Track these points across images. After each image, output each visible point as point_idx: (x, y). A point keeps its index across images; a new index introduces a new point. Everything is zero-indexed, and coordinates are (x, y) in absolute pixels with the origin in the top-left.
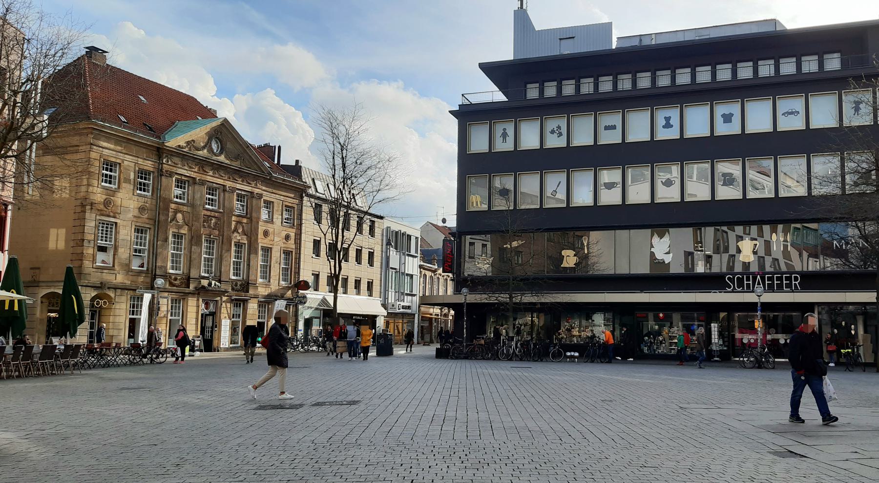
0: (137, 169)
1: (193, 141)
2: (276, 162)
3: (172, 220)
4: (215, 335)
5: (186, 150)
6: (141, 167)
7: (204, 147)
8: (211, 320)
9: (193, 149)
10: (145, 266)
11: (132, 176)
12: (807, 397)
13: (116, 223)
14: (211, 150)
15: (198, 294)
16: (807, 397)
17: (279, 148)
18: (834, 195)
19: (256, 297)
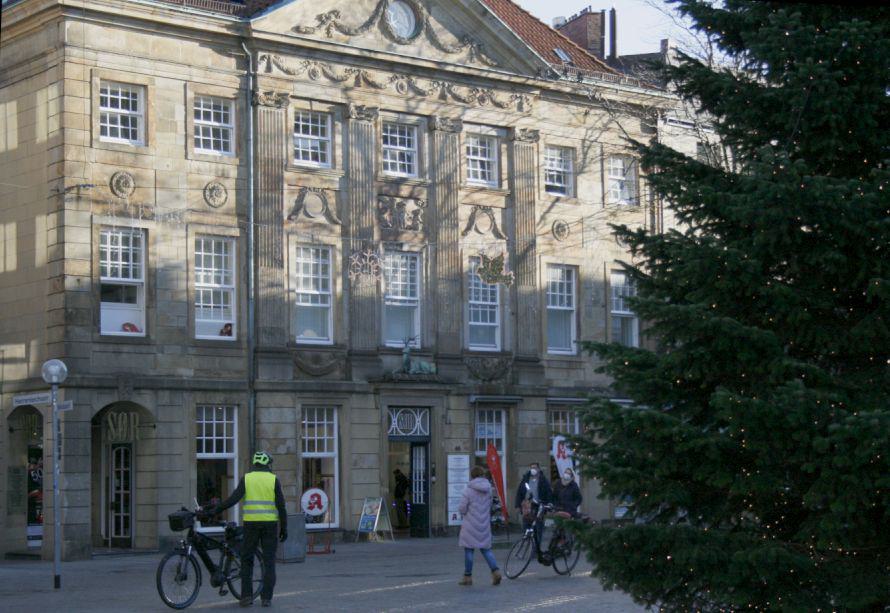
0: (191, 95)
1: (335, 13)
2: (607, 52)
3: (295, 211)
4: (436, 495)
5: (320, 35)
6: (204, 90)
7: (367, 25)
8: (422, 456)
9: (334, 32)
10: (234, 331)
11: (179, 117)
12: (621, 268)
13: (146, 231)
14: (386, 30)
15: (376, 392)
16: (621, 268)
17: (613, 12)
18: (243, 582)
19: (540, 393)
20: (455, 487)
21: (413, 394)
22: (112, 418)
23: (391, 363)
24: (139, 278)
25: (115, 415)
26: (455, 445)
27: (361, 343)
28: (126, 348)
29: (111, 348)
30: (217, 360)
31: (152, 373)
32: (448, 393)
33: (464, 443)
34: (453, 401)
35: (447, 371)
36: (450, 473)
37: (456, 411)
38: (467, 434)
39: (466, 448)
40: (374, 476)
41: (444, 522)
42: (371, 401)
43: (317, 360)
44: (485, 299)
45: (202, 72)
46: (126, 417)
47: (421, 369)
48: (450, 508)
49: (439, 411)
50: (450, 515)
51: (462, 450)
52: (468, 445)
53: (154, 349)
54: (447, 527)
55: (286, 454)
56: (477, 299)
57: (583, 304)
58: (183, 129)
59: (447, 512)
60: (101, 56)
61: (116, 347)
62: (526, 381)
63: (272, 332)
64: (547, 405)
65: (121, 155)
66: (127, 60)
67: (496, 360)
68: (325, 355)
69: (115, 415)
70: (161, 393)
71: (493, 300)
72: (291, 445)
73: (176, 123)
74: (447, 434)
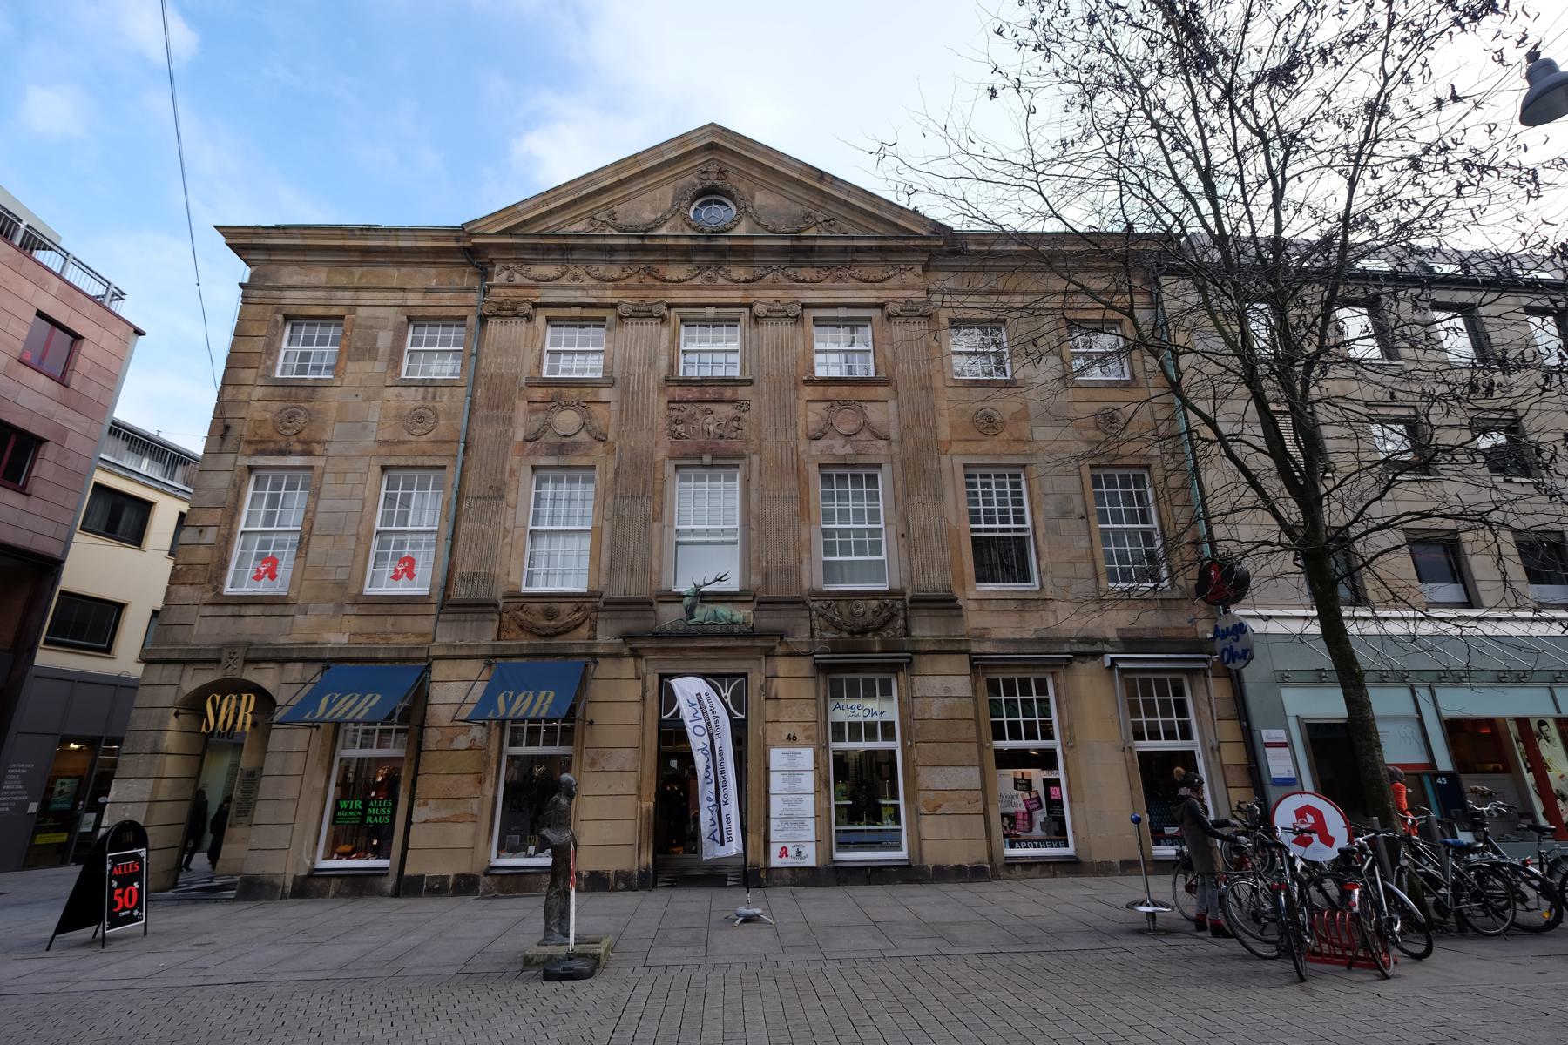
15: (636, 654)
20: (785, 801)
21: (696, 655)
22: (214, 700)
23: (670, 615)
24: (106, 650)
25: (218, 698)
26: (786, 730)
27: (625, 587)
28: (250, 611)
29: (228, 610)
30: (390, 620)
31: (283, 640)
32: (769, 653)
33: (805, 730)
34: (782, 665)
35: (769, 621)
36: (774, 777)
37: (790, 680)
38: (810, 714)
39: (807, 738)
40: (629, 783)
41: (762, 862)
42: (628, 667)
43: (550, 614)
44: (1005, 520)
45: (420, 295)
46: (234, 701)
47: (716, 618)
48: (774, 836)
49: (756, 680)
50: (775, 850)
51: (801, 739)
52: (813, 732)
53: (293, 610)
54: (769, 870)
55: (469, 749)
56: (990, 520)
57: (1040, 518)
58: (169, 668)
59: (767, 842)
60: (287, 293)
61: (236, 610)
62: (925, 629)
63: (472, 579)
64: (972, 666)
65: (294, 390)
66: (320, 294)
67: (874, 603)
68: (565, 608)
69: (218, 698)
70: (289, 666)
71: (1020, 520)
72: (479, 735)
73: (377, 350)
74: (770, 715)
